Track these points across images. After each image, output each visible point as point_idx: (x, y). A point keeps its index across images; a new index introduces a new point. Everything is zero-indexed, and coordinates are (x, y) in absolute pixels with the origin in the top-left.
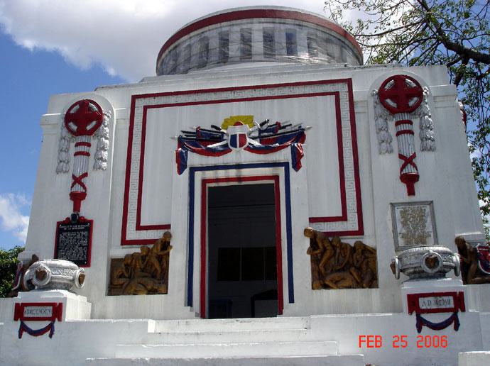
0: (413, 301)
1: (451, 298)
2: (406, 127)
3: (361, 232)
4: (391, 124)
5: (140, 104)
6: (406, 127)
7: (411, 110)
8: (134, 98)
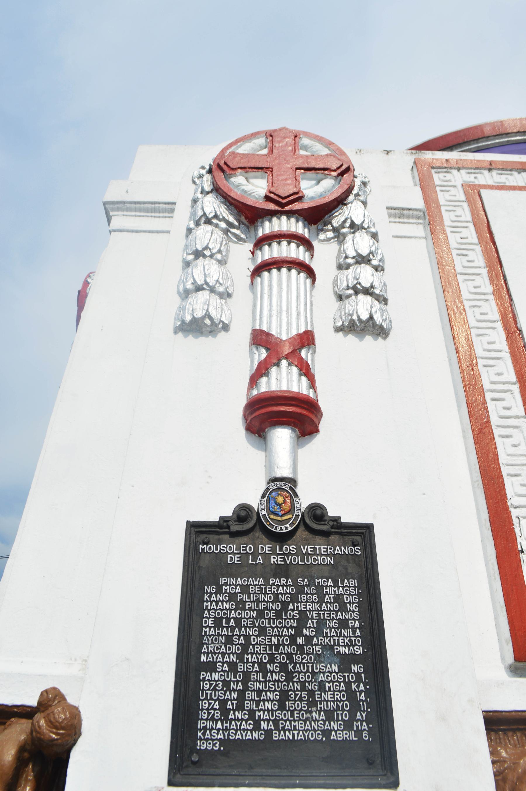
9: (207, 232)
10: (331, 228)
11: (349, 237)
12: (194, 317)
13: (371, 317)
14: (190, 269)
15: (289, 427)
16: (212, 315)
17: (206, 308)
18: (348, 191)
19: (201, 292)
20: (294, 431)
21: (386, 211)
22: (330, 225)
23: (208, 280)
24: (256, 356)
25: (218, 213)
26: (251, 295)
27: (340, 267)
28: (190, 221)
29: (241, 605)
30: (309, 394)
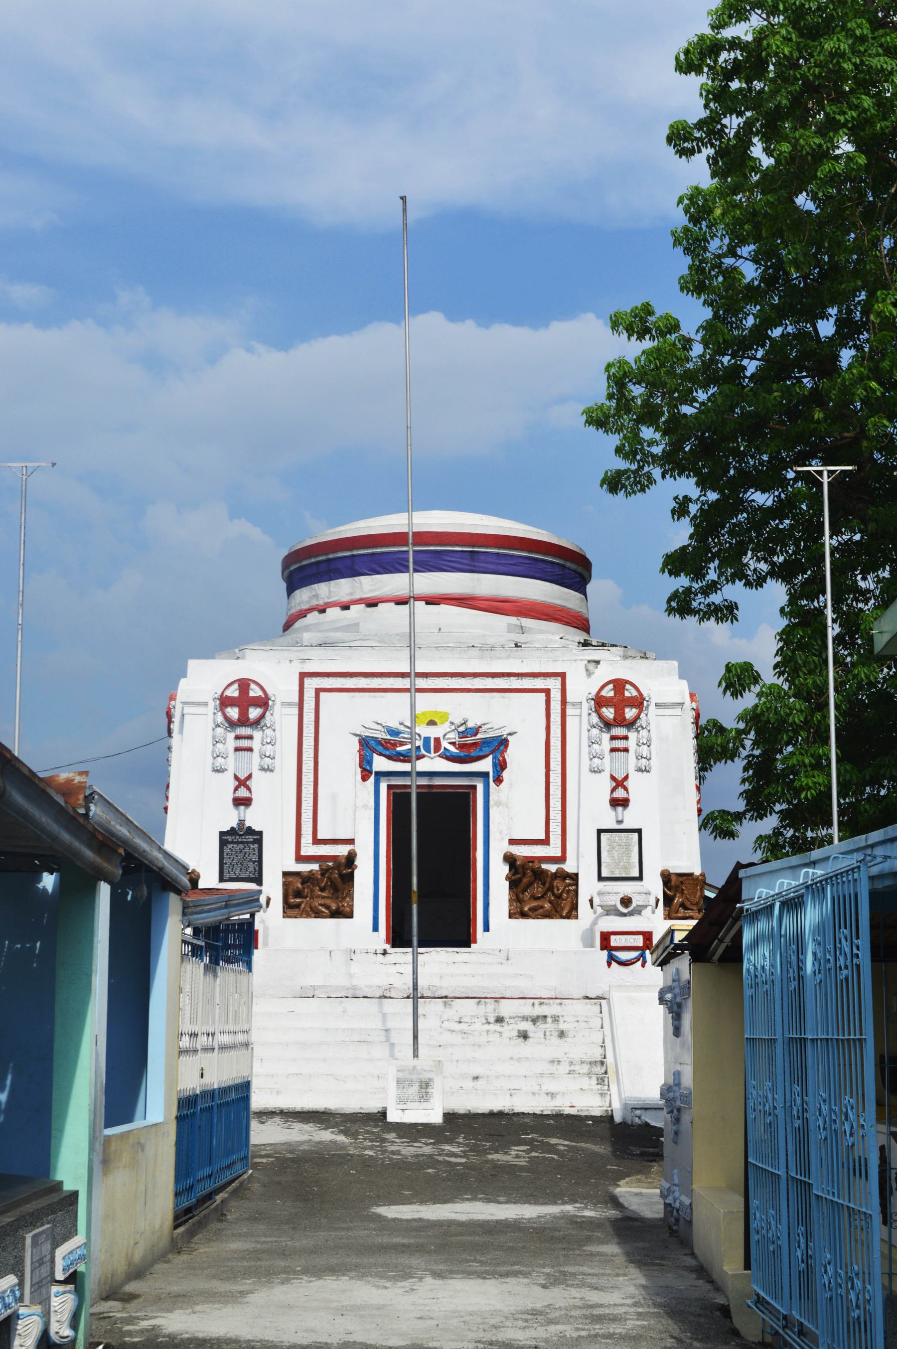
0: (605, 938)
1: (641, 937)
2: (245, 743)
3: (562, 859)
4: (231, 736)
5: (554, 685)
6: (245, 743)
7: (631, 725)
8: (303, 676)
29: (232, 851)
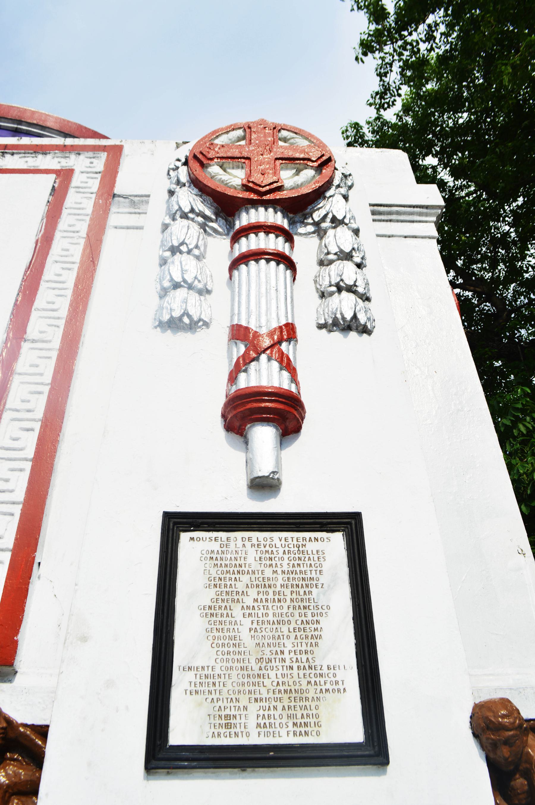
9: (184, 226)
10: (312, 221)
11: (331, 232)
12: (172, 317)
13: (355, 317)
14: (167, 267)
15: (271, 424)
16: (190, 313)
17: (184, 307)
18: (328, 185)
19: (179, 290)
20: (277, 429)
21: (369, 209)
22: (311, 219)
23: (186, 277)
24: (235, 349)
25: (195, 207)
26: (228, 292)
27: (321, 263)
28: (166, 216)
30: (291, 388)
